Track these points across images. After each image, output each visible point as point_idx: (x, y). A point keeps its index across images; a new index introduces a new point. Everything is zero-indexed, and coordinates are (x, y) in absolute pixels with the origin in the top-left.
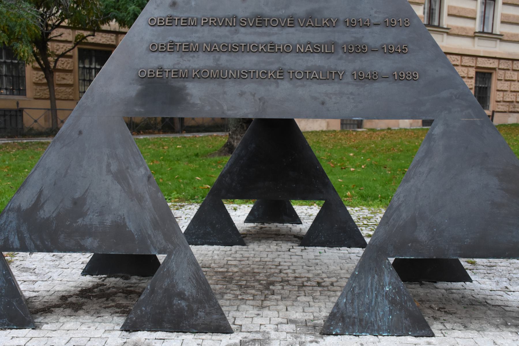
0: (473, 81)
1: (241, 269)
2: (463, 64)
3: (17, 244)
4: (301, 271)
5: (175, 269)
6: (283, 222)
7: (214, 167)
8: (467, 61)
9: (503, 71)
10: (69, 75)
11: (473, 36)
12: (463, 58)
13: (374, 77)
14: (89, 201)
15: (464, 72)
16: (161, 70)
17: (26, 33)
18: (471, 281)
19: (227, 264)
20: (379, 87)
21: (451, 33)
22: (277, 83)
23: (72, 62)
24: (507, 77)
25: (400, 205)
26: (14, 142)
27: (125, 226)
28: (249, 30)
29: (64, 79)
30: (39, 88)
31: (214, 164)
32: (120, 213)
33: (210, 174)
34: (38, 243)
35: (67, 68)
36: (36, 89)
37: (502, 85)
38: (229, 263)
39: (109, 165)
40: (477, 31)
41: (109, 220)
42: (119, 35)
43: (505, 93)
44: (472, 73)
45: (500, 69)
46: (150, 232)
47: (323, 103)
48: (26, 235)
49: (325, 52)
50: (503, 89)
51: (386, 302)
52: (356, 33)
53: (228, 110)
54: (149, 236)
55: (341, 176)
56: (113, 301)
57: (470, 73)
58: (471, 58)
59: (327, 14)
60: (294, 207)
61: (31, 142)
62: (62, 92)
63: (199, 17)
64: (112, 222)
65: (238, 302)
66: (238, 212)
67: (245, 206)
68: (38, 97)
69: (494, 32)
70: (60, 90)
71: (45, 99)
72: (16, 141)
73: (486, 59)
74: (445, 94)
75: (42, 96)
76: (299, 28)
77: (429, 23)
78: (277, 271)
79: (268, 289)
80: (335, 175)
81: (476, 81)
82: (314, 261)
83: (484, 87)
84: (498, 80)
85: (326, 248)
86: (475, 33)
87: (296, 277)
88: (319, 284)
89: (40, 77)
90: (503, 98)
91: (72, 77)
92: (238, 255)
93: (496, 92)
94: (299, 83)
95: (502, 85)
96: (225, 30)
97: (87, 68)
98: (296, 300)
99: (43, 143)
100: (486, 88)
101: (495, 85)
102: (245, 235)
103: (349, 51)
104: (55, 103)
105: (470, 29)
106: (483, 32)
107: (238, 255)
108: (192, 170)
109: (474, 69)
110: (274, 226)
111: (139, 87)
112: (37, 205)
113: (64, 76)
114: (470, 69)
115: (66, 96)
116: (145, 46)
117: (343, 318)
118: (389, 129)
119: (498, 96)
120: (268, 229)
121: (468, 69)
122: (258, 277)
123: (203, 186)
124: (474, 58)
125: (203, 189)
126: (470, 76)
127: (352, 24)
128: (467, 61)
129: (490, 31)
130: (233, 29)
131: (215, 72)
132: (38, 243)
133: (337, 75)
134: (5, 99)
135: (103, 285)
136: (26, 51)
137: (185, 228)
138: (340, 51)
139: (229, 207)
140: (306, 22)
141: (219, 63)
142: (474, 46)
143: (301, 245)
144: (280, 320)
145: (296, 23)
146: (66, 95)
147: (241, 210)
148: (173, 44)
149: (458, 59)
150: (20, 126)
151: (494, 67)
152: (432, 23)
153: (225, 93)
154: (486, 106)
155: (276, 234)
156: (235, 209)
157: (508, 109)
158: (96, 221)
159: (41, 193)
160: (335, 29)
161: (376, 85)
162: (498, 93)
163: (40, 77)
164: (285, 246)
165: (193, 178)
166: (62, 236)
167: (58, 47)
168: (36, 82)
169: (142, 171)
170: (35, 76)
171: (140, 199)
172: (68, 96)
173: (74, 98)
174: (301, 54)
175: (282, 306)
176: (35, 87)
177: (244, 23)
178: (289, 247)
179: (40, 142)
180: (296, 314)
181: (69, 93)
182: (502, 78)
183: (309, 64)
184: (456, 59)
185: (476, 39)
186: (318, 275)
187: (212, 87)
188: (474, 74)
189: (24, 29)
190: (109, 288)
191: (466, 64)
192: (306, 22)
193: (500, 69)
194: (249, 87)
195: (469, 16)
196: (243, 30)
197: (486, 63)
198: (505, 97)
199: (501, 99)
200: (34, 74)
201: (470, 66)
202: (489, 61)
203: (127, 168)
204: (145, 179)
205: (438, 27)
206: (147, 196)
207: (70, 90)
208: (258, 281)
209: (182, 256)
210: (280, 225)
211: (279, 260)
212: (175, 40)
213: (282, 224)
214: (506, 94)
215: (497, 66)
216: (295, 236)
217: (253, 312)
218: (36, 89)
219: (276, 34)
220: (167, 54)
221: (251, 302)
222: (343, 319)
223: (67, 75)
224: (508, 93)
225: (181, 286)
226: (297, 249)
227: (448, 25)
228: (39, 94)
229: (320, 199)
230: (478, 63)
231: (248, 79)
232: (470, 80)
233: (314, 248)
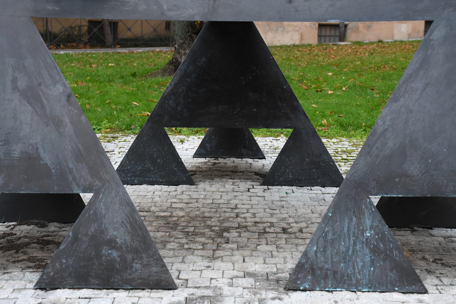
1: (189, 213)
3: (118, 169)
4: (261, 215)
5: (103, 211)
6: (241, 156)
7: (156, 91)
25: (386, 130)
27: (39, 158)
38: (174, 205)
39: (14, 80)
51: (367, 251)
53: (169, 10)
54: (71, 171)
56: (25, 253)
64: (22, 153)
65: (184, 252)
66: (186, 145)
67: (194, 137)
78: (233, 215)
79: (221, 236)
80: (308, 99)
85: (294, 188)
87: (256, 223)
88: (284, 230)
98: (255, 250)
102: (194, 173)
108: (128, 94)
110: (230, 162)
117: (313, 270)
118: (380, 41)
139: (174, 139)
144: (235, 273)
147: (189, 143)
155: (233, 171)
156: (182, 142)
164: (243, 185)
165: (128, 104)
175: (238, 257)
186: (284, 219)
190: (20, 238)
203: (40, 84)
206: (67, 120)
208: (210, 227)
209: (113, 194)
211: (236, 202)
216: (256, 174)
221: (200, 252)
222: (313, 271)
225: (112, 233)
226: (259, 189)
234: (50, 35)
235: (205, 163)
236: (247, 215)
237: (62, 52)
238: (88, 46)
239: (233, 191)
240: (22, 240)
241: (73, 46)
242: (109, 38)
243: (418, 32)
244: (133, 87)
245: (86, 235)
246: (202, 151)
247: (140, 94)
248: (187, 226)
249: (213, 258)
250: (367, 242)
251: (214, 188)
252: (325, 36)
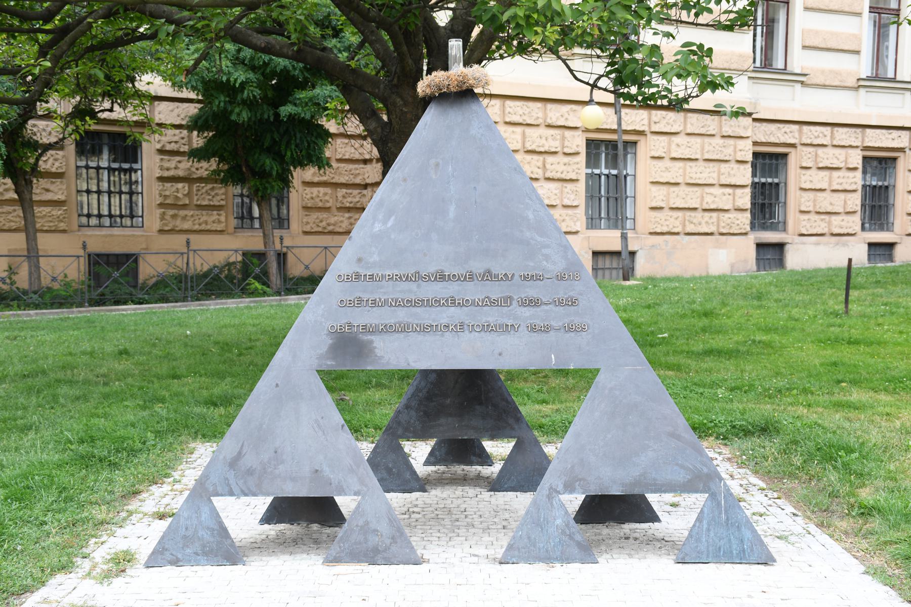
2: (835, 143)
6: (471, 463)
8: (843, 136)
10: (58, 183)
11: (856, 86)
12: (835, 132)
13: (546, 329)
15: (838, 159)
21: (809, 82)
23: (64, 157)
29: (47, 190)
35: (54, 170)
42: (156, 103)
49: (501, 305)
57: (850, 160)
58: (853, 130)
60: (483, 443)
62: (45, 216)
71: (16, 230)
73: (884, 131)
75: (4, 225)
81: (864, 172)
82: (503, 507)
85: (518, 493)
91: (64, 187)
100: (887, 187)
104: (35, 239)
106: (876, 78)
110: (459, 469)
111: (331, 342)
113: (48, 186)
114: (850, 151)
115: (51, 224)
124: (859, 130)
126: (851, 166)
128: (844, 136)
131: (400, 326)
133: (513, 328)
140: (484, 275)
143: (490, 490)
144: (464, 555)
145: (475, 278)
146: (51, 221)
149: (826, 133)
151: (902, 146)
164: (471, 491)
172: (56, 223)
173: (67, 229)
177: (427, 278)
181: (58, 217)
184: (822, 133)
185: (862, 91)
188: (861, 161)
195: (846, 48)
197: (884, 138)
201: (851, 146)
205: (784, 71)
207: (60, 212)
213: (469, 467)
223: (53, 183)
226: (486, 495)
227: (802, 68)
230: (866, 140)
231: (431, 332)
232: (851, 174)
233: (505, 493)
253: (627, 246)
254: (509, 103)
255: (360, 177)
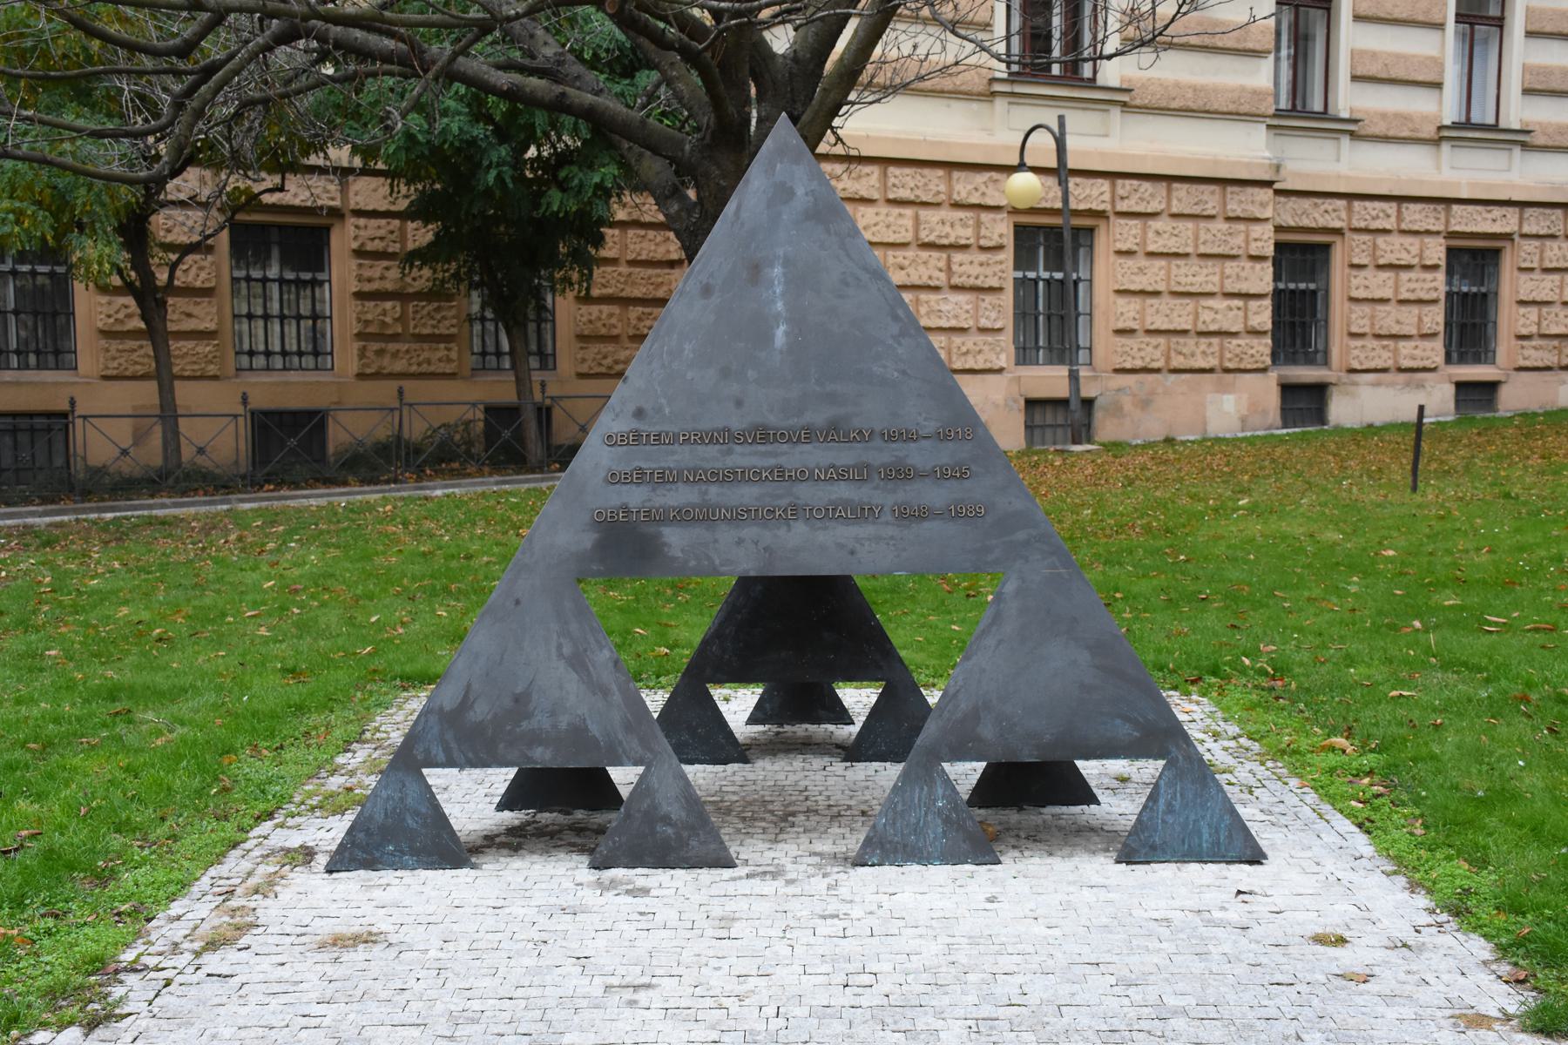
0: (1441, 276)
1: (744, 797)
2: (1404, 226)
3: (441, 757)
4: (837, 797)
5: (656, 786)
6: (818, 721)
7: (669, 601)
8: (1416, 216)
9: (1536, 243)
11: (1436, 137)
13: (922, 514)
14: (535, 696)
15: (1409, 252)
16: (626, 509)
17: (103, 205)
18: (1099, 804)
19: (720, 791)
20: (930, 528)
21: (1363, 132)
22: (789, 526)
23: (212, 263)
24: (1551, 261)
25: (958, 691)
26: (77, 520)
27: (586, 729)
28: (747, 449)
29: (189, 315)
30: (115, 345)
31: (669, 592)
32: (579, 712)
33: (664, 620)
34: (470, 755)
35: (198, 284)
36: (107, 350)
37: (1529, 287)
38: (724, 789)
39: (559, 647)
40: (1447, 122)
41: (564, 722)
43: (1545, 310)
44: (1436, 251)
45: (1524, 236)
46: (620, 737)
47: (852, 553)
48: (453, 745)
50: (1538, 299)
51: (939, 822)
52: (898, 450)
53: (722, 565)
54: (620, 743)
55: (962, 615)
56: (561, 839)
57: (1427, 253)
59: (857, 423)
61: (126, 518)
63: (676, 431)
64: (569, 724)
65: (742, 837)
66: (733, 705)
67: (745, 691)
68: (115, 372)
69: (1502, 125)
70: (179, 349)
71: (144, 377)
72: (84, 516)
73: (1479, 208)
74: (1021, 535)
75: (126, 369)
76: (817, 444)
77: (1294, 105)
78: (801, 798)
79: (786, 821)
80: (950, 613)
81: (1450, 272)
83: (1475, 295)
84: (1521, 269)
85: (888, 764)
86: (1440, 128)
87: (830, 806)
88: (864, 813)
89: (117, 312)
90: (1539, 324)
91: (214, 310)
92: (738, 778)
93: (1515, 306)
94: (819, 524)
95: (1529, 287)
96: (712, 450)
97: (256, 280)
98: (826, 832)
99: (163, 522)
100: (1485, 295)
101: (1513, 285)
102: (749, 747)
103: (887, 478)
105: (1425, 118)
107: (738, 778)
108: (621, 609)
109: (1442, 241)
110: (801, 730)
112: (465, 704)
113: (191, 309)
114: (1428, 240)
115: (196, 367)
116: (603, 474)
117: (881, 843)
118: (1169, 441)
119: (1521, 322)
120: (789, 734)
121: (1422, 242)
122: (770, 807)
123: (653, 651)
124: (1440, 207)
125: (655, 657)
126: (1429, 263)
127: (891, 437)
128: (1417, 216)
129: (1491, 120)
130: (725, 447)
132: (470, 755)
134: (18, 384)
135: (534, 822)
136: (106, 258)
137: (504, 770)
138: (876, 476)
139: (717, 693)
140: (827, 436)
141: (707, 498)
142: (1438, 168)
143: (845, 760)
144: (800, 853)
146: (195, 363)
147: (738, 701)
148: (641, 472)
149: (1390, 211)
150: (59, 462)
151: (1508, 230)
152: (1304, 106)
153: (716, 541)
154: (1486, 352)
155: (804, 744)
156: (727, 700)
157: (1555, 359)
158: (546, 724)
159: (469, 686)
160: (870, 444)
161: (926, 525)
162: (1522, 310)
163: (117, 312)
164: (817, 762)
165: (628, 632)
166: (501, 746)
167: (170, 223)
168: (106, 328)
169: (606, 653)
170: (105, 310)
171: (605, 692)
174: (821, 483)
175: (804, 839)
176: (103, 343)
178: (823, 764)
179: (150, 517)
180: (825, 846)
182: (1535, 265)
183: (834, 497)
184: (1383, 211)
186: (866, 801)
187: (698, 533)
188: (1443, 255)
189: (98, 195)
190: (547, 826)
191: (1416, 228)
192: (827, 436)
193: (1524, 236)
194: (750, 532)
195: (1420, 78)
196: (738, 449)
198: (1544, 323)
199: (1534, 329)
200: (102, 305)
201: (1428, 232)
202: (1489, 211)
203: (585, 650)
204: (611, 665)
205: (1324, 115)
206: (614, 688)
207: (208, 349)
208: (772, 812)
209: (666, 766)
210: (812, 728)
211: (807, 783)
212: (643, 465)
214: (1548, 313)
215: (1516, 228)
216: (838, 746)
217: (761, 846)
218: (107, 350)
219: (786, 453)
220: (634, 487)
221: (761, 836)
222: (882, 846)
223: (197, 304)
224: (1556, 309)
225: (665, 808)
226: (839, 767)
227: (1352, 110)
228: (115, 364)
229: (877, 680)
230: (1453, 221)
234: (407, 447)
235: (764, 732)
236: (819, 798)
237: (439, 492)
238: (486, 469)
239: (803, 770)
240: (551, 828)
241: (453, 470)
242: (535, 449)
243: (1265, 412)
244: (627, 595)
245: (639, 811)
246: (760, 715)
247: (643, 611)
248: (743, 812)
249: (776, 841)
250: (940, 812)
251: (777, 767)
252: (1042, 427)
253: (1078, 390)
254: (892, 170)
255: (665, 288)
